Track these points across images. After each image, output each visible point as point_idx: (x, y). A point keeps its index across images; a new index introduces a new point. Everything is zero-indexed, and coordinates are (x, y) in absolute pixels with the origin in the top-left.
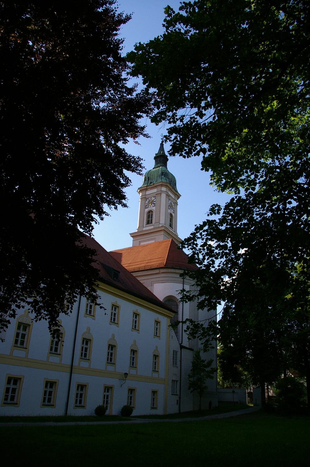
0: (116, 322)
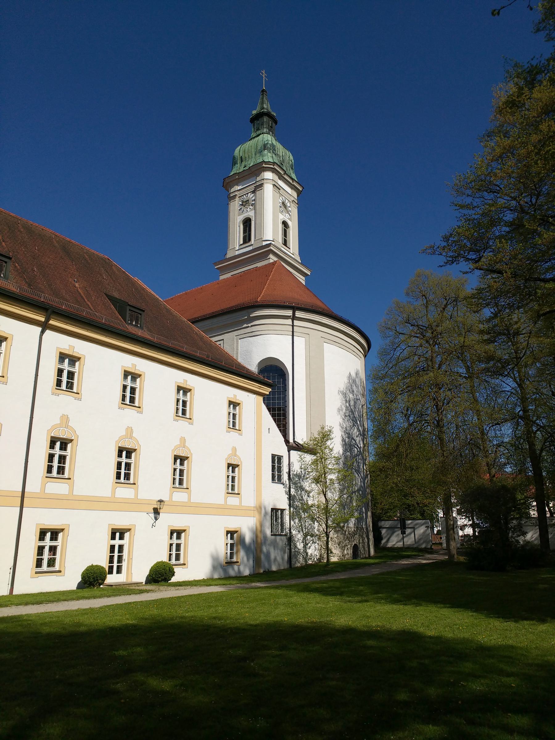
0: (237, 428)
